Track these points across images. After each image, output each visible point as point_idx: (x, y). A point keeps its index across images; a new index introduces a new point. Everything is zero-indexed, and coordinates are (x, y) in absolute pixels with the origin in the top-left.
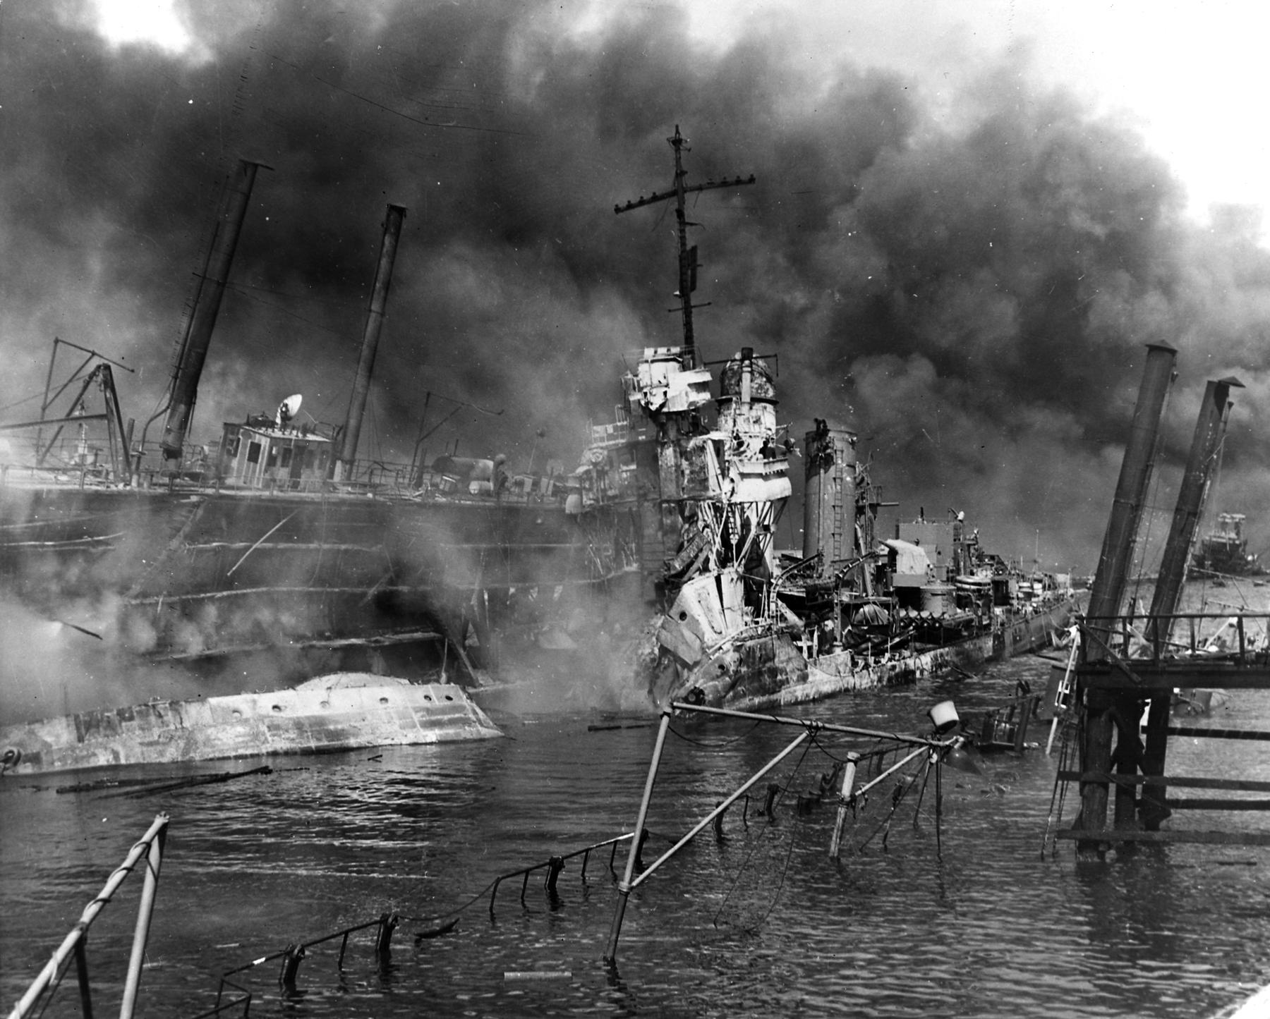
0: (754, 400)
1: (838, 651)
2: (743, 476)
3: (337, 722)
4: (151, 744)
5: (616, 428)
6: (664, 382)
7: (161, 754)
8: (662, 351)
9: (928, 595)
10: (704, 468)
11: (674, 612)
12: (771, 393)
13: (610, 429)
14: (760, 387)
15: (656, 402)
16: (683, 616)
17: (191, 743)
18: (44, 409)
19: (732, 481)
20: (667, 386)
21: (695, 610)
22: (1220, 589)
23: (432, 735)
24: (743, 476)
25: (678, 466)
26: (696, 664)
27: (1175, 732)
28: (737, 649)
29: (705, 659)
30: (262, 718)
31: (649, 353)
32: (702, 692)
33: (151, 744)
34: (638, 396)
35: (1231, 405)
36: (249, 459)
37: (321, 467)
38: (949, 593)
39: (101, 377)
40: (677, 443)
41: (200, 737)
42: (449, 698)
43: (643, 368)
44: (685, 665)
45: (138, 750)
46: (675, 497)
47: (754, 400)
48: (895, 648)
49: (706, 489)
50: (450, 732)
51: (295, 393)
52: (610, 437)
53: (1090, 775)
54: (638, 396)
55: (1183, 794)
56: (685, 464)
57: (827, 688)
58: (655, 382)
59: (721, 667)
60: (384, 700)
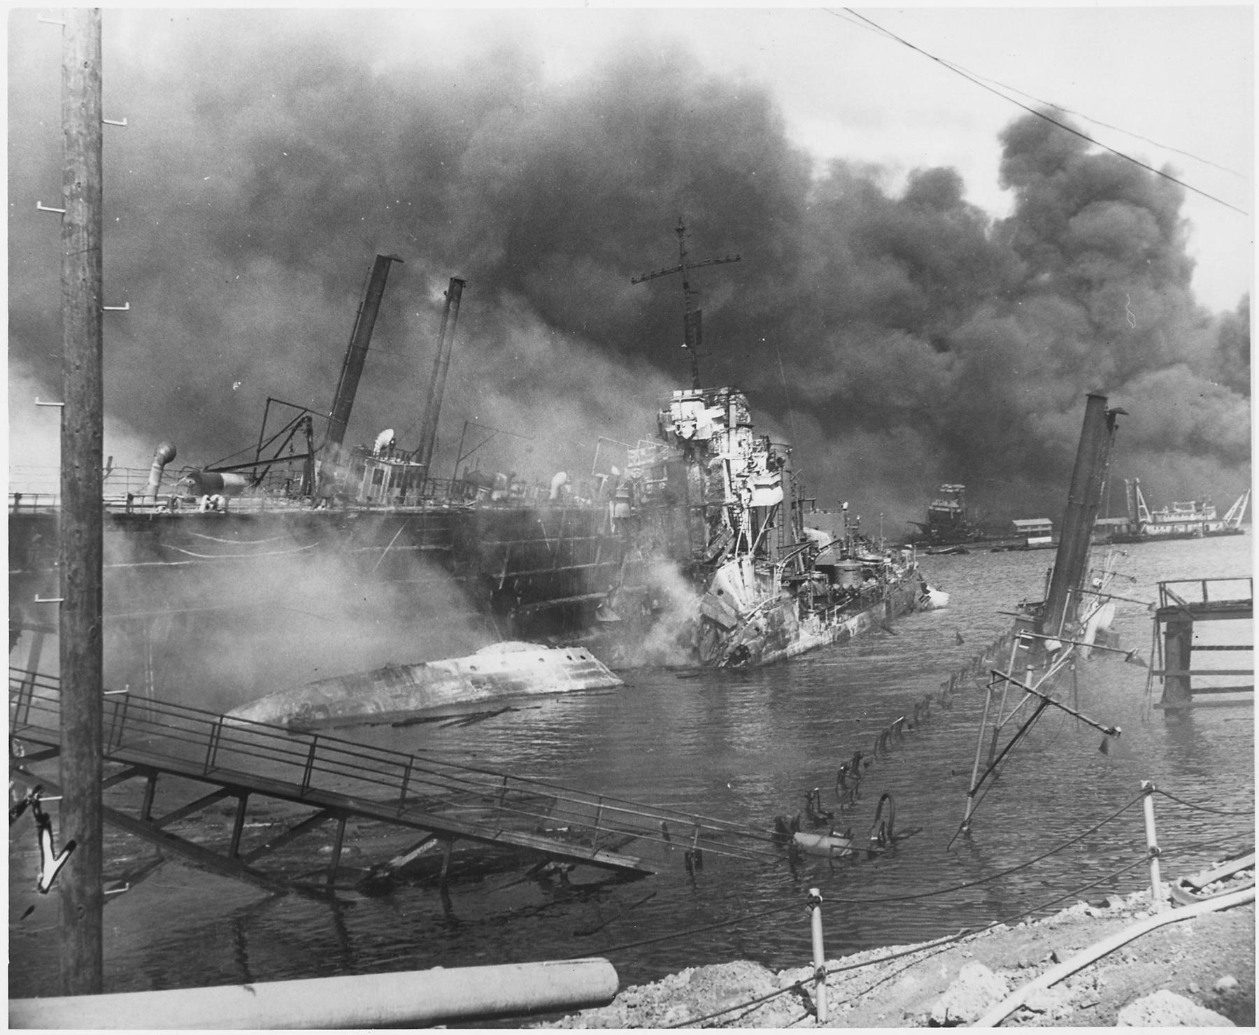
0: (739, 426)
1: (811, 616)
2: (757, 487)
3: (517, 677)
4: (397, 697)
5: (647, 452)
6: (692, 417)
7: (407, 703)
8: (688, 393)
9: (841, 571)
10: (721, 481)
11: (713, 589)
12: (749, 420)
13: (643, 452)
14: (742, 415)
15: (687, 435)
16: (720, 592)
17: (424, 696)
18: (259, 451)
19: (749, 490)
20: (695, 419)
21: (728, 587)
22: (962, 557)
23: (581, 684)
24: (757, 487)
25: (702, 480)
26: (734, 627)
27: (1194, 648)
28: (765, 615)
29: (741, 624)
30: (465, 676)
31: (677, 394)
32: (746, 648)
33: (397, 697)
34: (673, 428)
35: (1117, 427)
36: (374, 482)
37: (418, 486)
38: (858, 569)
39: (304, 426)
40: (701, 464)
41: (428, 690)
42: (583, 658)
43: (674, 406)
44: (724, 628)
45: (390, 701)
46: (701, 503)
47: (739, 426)
48: (839, 612)
49: (723, 496)
50: (592, 682)
51: (387, 428)
52: (643, 458)
53: (1170, 672)
54: (673, 428)
55: (1210, 681)
56: (706, 478)
57: (809, 645)
58: (685, 417)
59: (757, 629)
60: (541, 660)
